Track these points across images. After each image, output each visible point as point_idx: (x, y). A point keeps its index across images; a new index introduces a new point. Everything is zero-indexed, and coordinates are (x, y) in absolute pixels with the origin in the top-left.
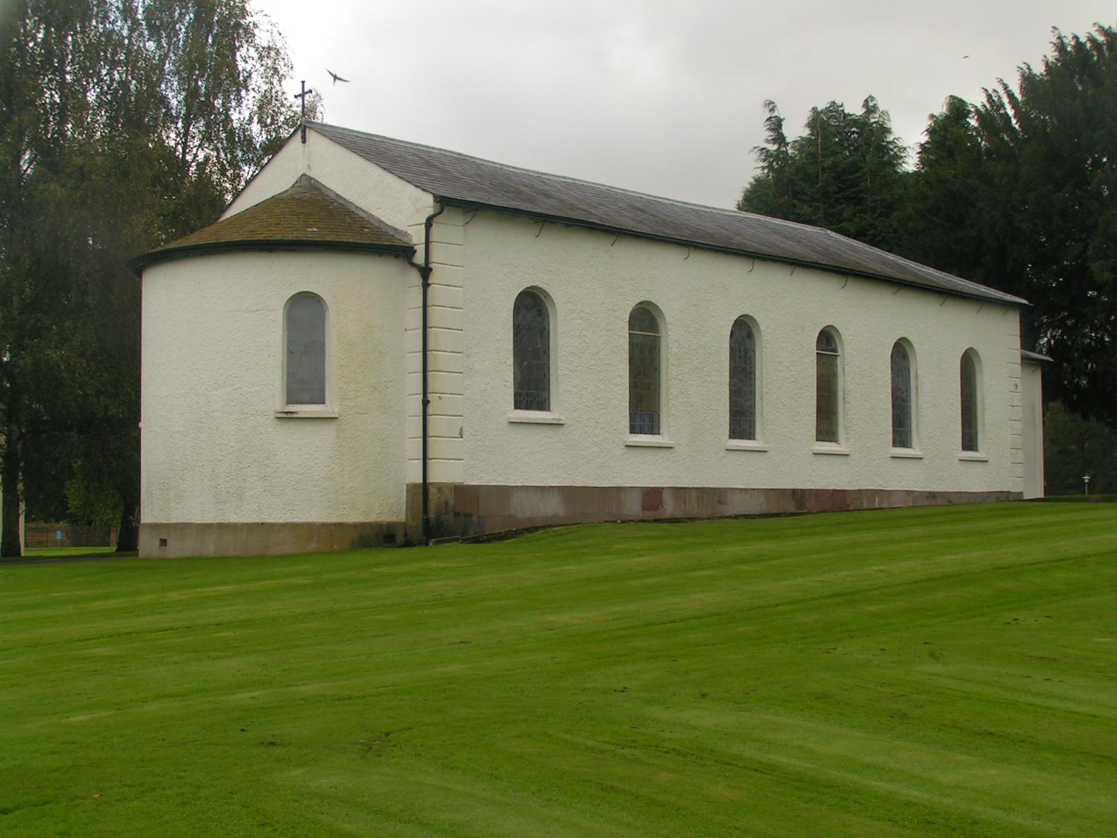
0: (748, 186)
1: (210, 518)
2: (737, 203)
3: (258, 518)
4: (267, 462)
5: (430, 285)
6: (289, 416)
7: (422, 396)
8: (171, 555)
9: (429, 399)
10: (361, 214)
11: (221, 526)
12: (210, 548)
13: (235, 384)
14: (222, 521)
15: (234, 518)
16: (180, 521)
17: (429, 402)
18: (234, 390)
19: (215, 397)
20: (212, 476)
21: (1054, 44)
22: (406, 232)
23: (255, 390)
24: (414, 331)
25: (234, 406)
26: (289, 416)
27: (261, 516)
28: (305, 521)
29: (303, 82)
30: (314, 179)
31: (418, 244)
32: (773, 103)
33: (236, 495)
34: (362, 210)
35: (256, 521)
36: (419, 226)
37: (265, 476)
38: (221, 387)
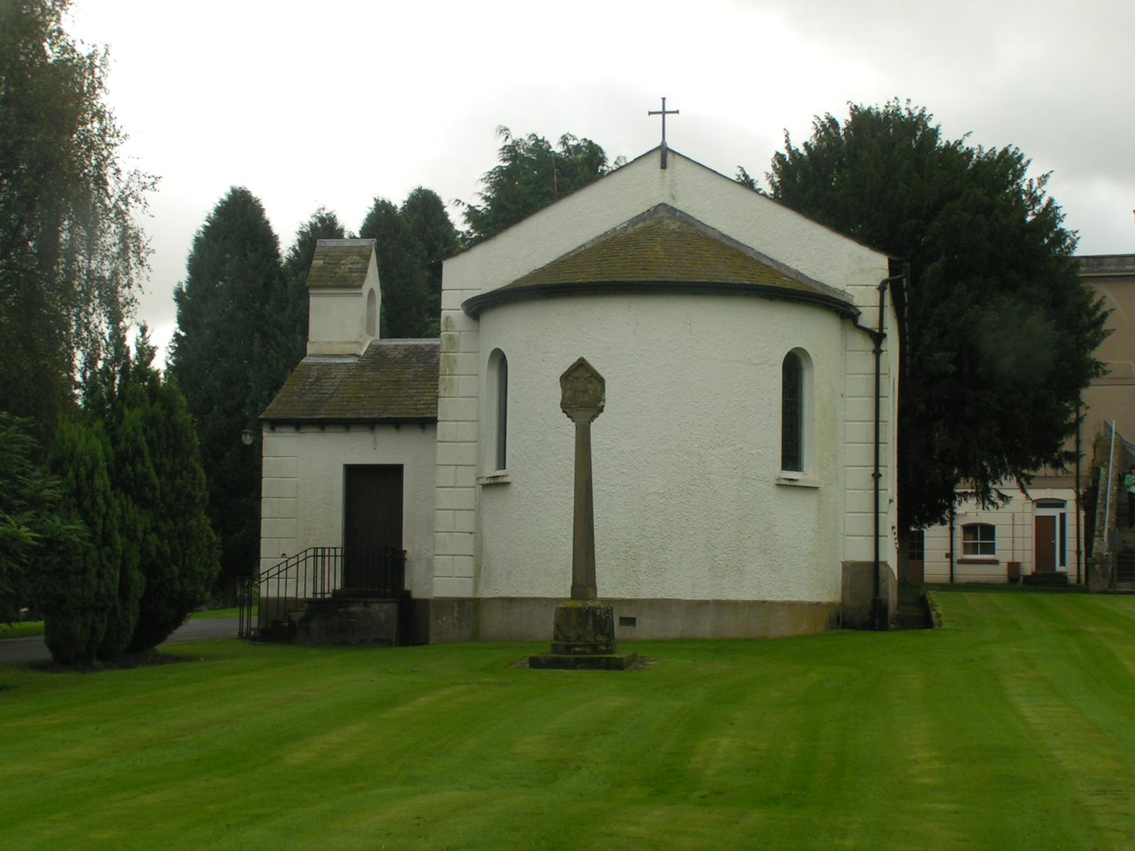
0: (225, 198)
1: (704, 593)
2: (207, 215)
3: (758, 595)
4: (767, 533)
5: (882, 351)
6: (792, 483)
7: (874, 468)
8: (644, 636)
9: (881, 472)
10: (764, 261)
11: (719, 604)
12: (705, 627)
13: (735, 445)
14: (719, 598)
15: (732, 596)
16: (658, 597)
17: (881, 475)
18: (735, 451)
19: (713, 457)
20: (707, 547)
21: (960, 143)
22: (844, 291)
23: (757, 452)
24: (858, 399)
25: (735, 469)
26: (792, 483)
27: (761, 593)
28: (797, 600)
29: (664, 99)
30: (681, 212)
31: (864, 306)
32: (507, 129)
33: (735, 569)
34: (767, 258)
35: (757, 599)
36: (865, 287)
37: (765, 549)
38: (719, 446)
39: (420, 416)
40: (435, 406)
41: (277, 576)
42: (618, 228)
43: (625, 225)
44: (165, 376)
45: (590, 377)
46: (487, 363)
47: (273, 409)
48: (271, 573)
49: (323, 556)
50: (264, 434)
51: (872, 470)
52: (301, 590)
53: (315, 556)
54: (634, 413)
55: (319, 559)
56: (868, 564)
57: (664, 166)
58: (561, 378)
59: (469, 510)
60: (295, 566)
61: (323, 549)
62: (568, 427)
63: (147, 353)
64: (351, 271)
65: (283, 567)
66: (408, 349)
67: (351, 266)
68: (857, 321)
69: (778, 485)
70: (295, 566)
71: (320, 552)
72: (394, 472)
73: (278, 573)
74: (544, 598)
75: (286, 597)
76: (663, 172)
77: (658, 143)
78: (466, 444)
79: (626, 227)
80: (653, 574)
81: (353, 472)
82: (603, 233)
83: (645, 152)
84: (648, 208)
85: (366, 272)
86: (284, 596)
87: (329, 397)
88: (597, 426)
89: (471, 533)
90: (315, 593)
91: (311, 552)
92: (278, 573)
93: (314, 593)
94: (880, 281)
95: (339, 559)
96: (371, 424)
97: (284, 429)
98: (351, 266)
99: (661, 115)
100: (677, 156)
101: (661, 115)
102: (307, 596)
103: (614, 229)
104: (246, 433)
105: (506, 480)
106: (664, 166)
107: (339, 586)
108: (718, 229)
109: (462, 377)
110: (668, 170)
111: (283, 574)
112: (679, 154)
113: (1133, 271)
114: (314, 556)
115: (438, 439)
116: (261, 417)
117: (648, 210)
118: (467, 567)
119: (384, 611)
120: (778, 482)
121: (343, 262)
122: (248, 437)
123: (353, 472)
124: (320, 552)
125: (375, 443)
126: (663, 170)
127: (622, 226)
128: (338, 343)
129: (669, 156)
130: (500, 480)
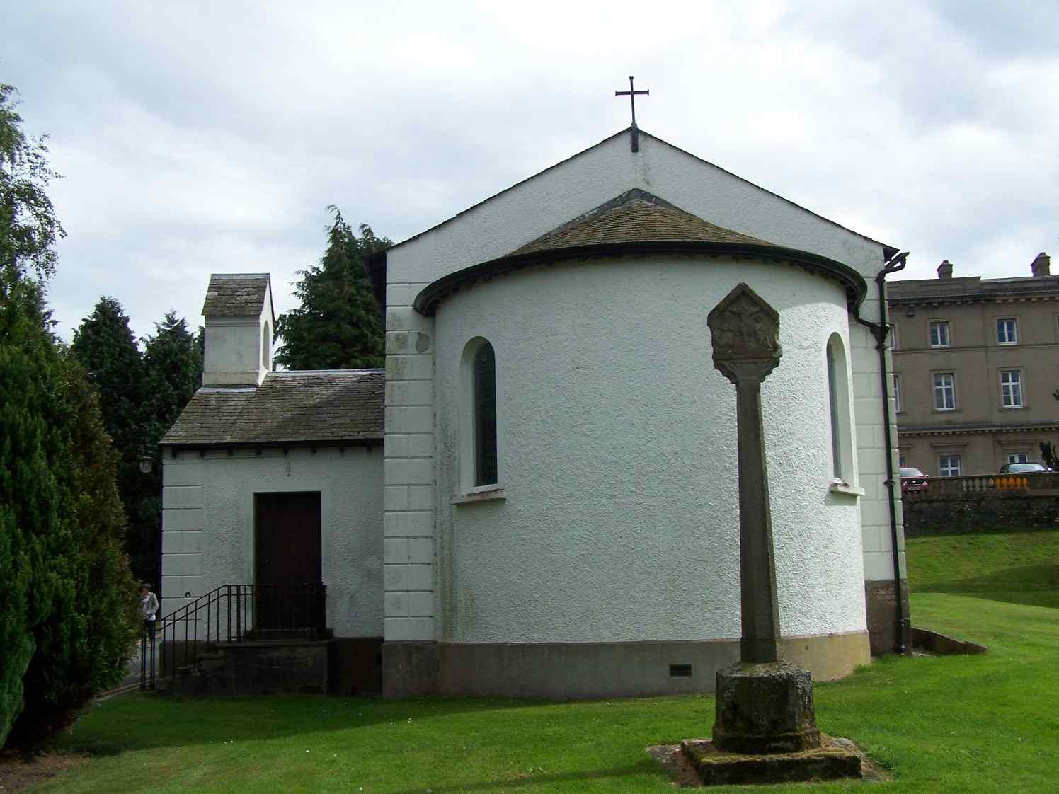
9: (894, 480)
29: (631, 78)
39: (339, 439)
40: (381, 421)
41: (185, 618)
42: (587, 215)
43: (595, 211)
44: (36, 445)
45: (758, 312)
46: (459, 360)
47: (176, 434)
48: (178, 616)
49: (238, 595)
50: (164, 461)
51: (885, 478)
52: (213, 631)
53: (230, 595)
54: (674, 406)
55: (234, 599)
56: (891, 581)
57: (635, 149)
58: (711, 316)
59: (426, 537)
60: (207, 606)
61: (238, 587)
62: (727, 393)
63: (43, 308)
64: (247, 301)
65: (192, 608)
66: (307, 379)
67: (247, 297)
68: (858, 315)
69: (831, 492)
70: (207, 606)
71: (234, 590)
72: (313, 499)
73: (187, 616)
74: (563, 644)
75: (195, 641)
76: (636, 156)
77: (629, 125)
78: (420, 460)
79: (596, 214)
80: (709, 608)
81: (264, 502)
82: (570, 220)
83: (615, 134)
84: (620, 194)
85: (263, 303)
86: (193, 639)
87: (233, 423)
88: (771, 387)
89: (429, 564)
90: (230, 637)
91: (224, 591)
92: (187, 616)
93: (228, 638)
94: (878, 273)
95: (249, 597)
96: (285, 448)
97: (187, 456)
98: (247, 297)
99: (634, 90)
100: (649, 139)
101: (635, 96)
102: (221, 639)
103: (583, 216)
104: (143, 461)
105: (499, 495)
106: (635, 149)
107: (249, 626)
108: (698, 216)
109: (413, 382)
110: (639, 154)
111: (192, 616)
112: (651, 136)
113: (1056, 287)
114: (231, 595)
115: (385, 455)
116: (161, 442)
117: (621, 196)
118: (425, 604)
119: (310, 655)
120: (833, 489)
121: (239, 293)
122: (147, 464)
123: (264, 502)
124: (234, 590)
125: (289, 470)
126: (634, 153)
127: (591, 213)
128: (235, 374)
129: (641, 139)
130: (494, 496)
